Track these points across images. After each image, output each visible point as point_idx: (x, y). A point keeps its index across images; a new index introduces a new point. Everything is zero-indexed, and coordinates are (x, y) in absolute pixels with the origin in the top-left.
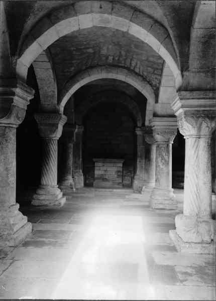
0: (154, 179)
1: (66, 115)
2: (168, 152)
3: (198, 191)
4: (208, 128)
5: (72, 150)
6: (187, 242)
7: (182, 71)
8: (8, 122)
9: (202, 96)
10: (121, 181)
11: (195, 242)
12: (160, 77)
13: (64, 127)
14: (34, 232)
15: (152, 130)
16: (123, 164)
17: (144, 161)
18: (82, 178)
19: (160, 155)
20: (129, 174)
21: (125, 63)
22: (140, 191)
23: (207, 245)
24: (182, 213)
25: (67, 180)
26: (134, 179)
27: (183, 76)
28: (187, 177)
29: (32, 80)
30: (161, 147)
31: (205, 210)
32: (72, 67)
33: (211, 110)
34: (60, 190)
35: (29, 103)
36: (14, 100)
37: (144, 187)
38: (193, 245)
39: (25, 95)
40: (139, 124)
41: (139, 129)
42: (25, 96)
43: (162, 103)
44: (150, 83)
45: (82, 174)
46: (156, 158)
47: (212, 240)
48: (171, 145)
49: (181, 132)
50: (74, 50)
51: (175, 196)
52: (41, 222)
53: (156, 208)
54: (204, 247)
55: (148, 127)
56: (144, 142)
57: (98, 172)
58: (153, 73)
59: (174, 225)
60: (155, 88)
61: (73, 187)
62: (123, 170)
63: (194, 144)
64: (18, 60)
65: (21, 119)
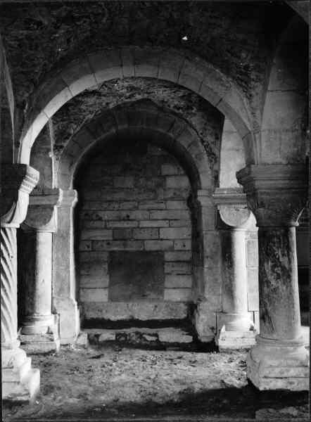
1: (36, 168)
2: (289, 248)
17: (219, 265)
19: (268, 255)
25: (37, 320)
61: (55, 336)
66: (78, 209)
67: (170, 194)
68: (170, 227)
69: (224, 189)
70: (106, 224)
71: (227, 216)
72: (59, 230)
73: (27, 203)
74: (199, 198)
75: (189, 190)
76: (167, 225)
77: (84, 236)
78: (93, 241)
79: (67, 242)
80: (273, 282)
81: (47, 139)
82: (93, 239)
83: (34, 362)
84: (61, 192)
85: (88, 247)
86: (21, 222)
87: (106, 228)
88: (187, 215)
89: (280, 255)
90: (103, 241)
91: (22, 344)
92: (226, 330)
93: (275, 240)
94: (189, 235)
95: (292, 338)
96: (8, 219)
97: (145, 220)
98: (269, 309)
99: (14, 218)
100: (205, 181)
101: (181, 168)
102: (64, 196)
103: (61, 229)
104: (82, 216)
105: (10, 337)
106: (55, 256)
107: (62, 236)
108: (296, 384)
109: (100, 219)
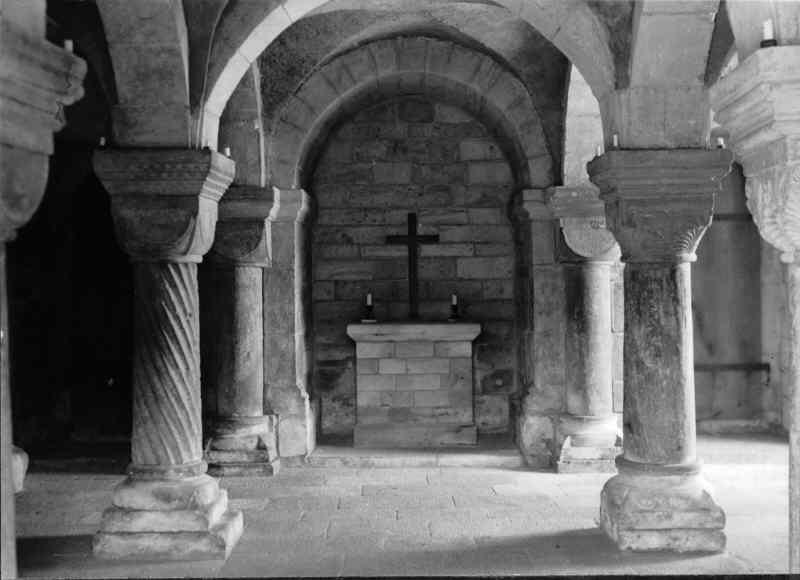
57: (368, 392)
60: (612, 22)
66: (310, 222)
67: (476, 195)
68: (475, 256)
69: (570, 190)
70: (359, 250)
71: (577, 239)
72: (274, 263)
73: (215, 218)
74: (526, 206)
75: (510, 188)
76: (471, 254)
77: (323, 271)
78: (336, 282)
79: (290, 286)
80: (648, 363)
81: (251, 95)
82: (337, 278)
84: (277, 192)
85: (329, 293)
86: (205, 251)
87: (360, 258)
88: (506, 233)
89: (662, 314)
90: (355, 282)
91: (211, 466)
92: (572, 445)
93: (654, 286)
94: (510, 272)
95: (679, 459)
96: (183, 248)
99: (193, 246)
100: (538, 172)
101: (496, 148)
102: (282, 201)
103: (278, 260)
104: (317, 233)
105: (191, 457)
106: (268, 309)
107: (280, 273)
108: (684, 540)
109: (349, 241)
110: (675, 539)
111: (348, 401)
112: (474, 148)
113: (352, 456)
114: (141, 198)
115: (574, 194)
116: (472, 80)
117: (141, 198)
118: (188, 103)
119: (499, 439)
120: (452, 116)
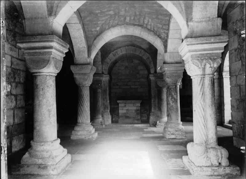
0: (166, 115)
2: (176, 92)
3: (205, 122)
4: (211, 68)
5: (101, 95)
6: (199, 166)
7: (187, 22)
8: (49, 72)
9: (204, 42)
10: (139, 118)
11: (206, 166)
12: (167, 31)
13: (94, 76)
14: (73, 162)
15: (163, 75)
16: (141, 104)
18: (110, 116)
19: (170, 94)
20: (145, 112)
21: (139, 21)
22: (155, 125)
23: (216, 168)
24: (193, 141)
25: (98, 118)
26: (150, 115)
27: (188, 26)
28: (195, 111)
29: (66, 36)
30: (171, 88)
31: (212, 138)
32: (97, 27)
33: (213, 53)
34: (93, 127)
35: (65, 56)
36: (52, 53)
37: (158, 122)
38: (205, 169)
39: (62, 49)
40: (152, 71)
41: (152, 75)
42: (61, 50)
43: (170, 52)
44: (160, 36)
45: (110, 113)
46: (167, 97)
47: (220, 164)
48: (178, 86)
49: (189, 73)
50: (99, 13)
51: (183, 127)
52: (79, 153)
53: (169, 138)
54: (213, 170)
55: (159, 73)
56: (157, 86)
57: (121, 111)
58: (162, 28)
59: (187, 151)
60: (164, 41)
62: (141, 109)
63: (200, 82)
64: (54, 20)
65: (59, 69)
74: (150, 77)
83: (124, 114)
92: (159, 122)
97: (133, 85)
98: (170, 112)
105: (105, 77)
109: (117, 85)
110: (177, 136)
111: (118, 115)
112: (140, 67)
113: (118, 125)
114: (79, 74)
115: (159, 75)
116: (140, 54)
117: (79, 74)
118: (87, 56)
119: (147, 122)
120: (136, 61)
